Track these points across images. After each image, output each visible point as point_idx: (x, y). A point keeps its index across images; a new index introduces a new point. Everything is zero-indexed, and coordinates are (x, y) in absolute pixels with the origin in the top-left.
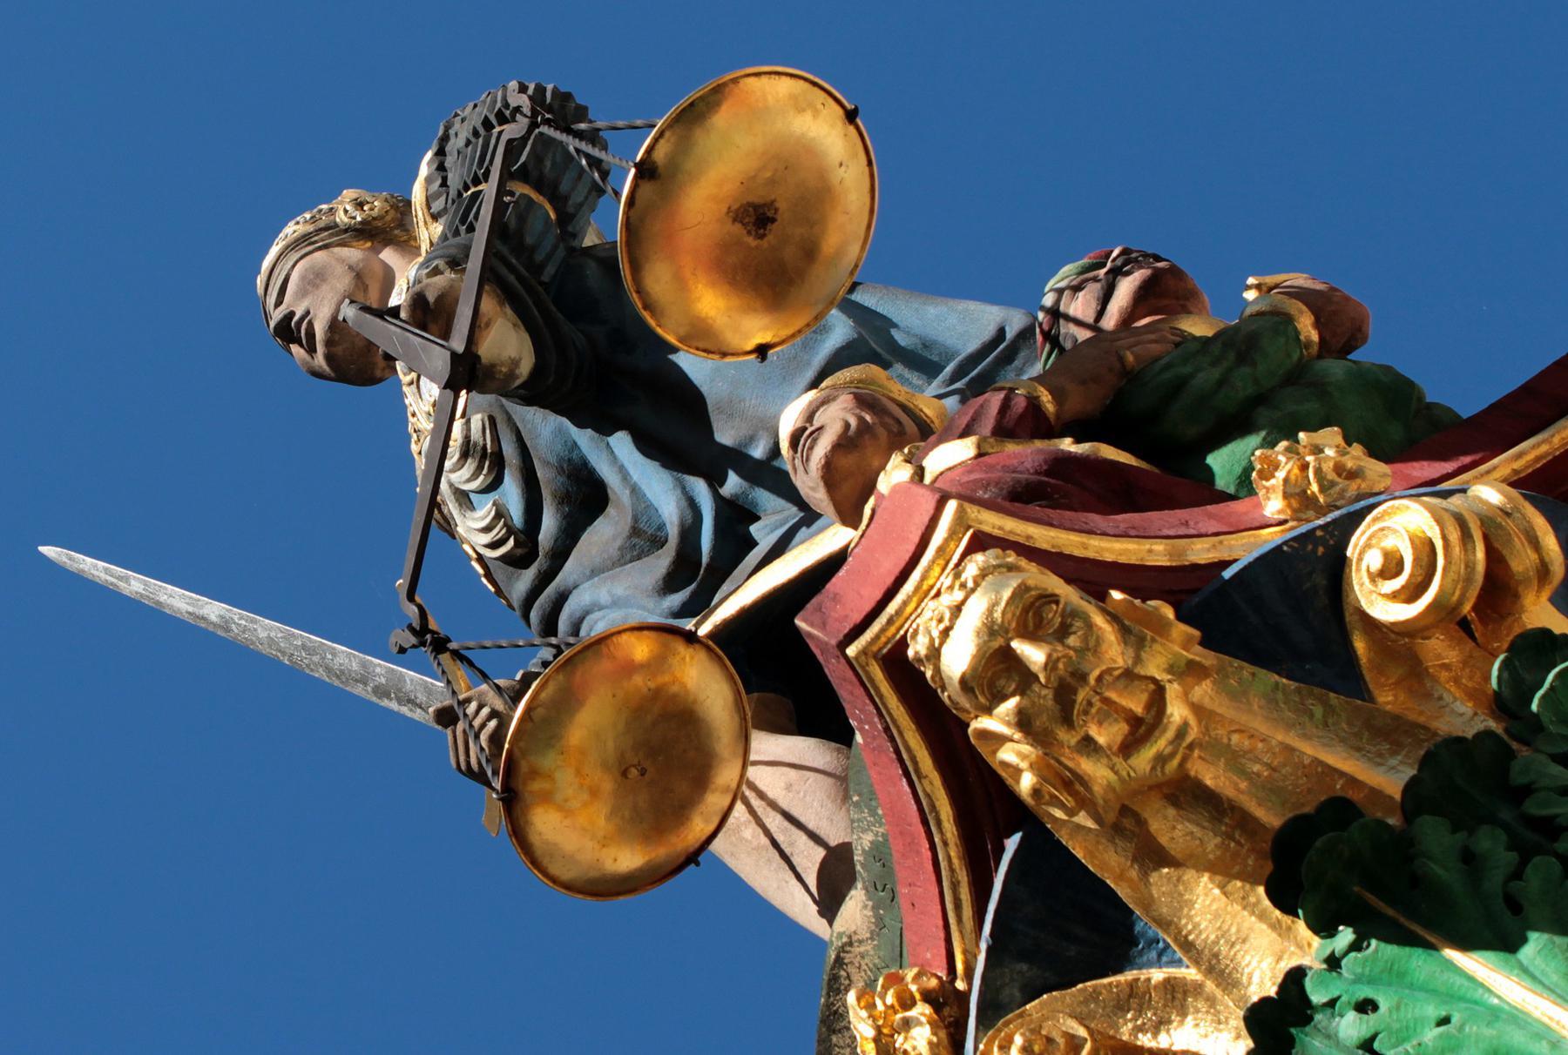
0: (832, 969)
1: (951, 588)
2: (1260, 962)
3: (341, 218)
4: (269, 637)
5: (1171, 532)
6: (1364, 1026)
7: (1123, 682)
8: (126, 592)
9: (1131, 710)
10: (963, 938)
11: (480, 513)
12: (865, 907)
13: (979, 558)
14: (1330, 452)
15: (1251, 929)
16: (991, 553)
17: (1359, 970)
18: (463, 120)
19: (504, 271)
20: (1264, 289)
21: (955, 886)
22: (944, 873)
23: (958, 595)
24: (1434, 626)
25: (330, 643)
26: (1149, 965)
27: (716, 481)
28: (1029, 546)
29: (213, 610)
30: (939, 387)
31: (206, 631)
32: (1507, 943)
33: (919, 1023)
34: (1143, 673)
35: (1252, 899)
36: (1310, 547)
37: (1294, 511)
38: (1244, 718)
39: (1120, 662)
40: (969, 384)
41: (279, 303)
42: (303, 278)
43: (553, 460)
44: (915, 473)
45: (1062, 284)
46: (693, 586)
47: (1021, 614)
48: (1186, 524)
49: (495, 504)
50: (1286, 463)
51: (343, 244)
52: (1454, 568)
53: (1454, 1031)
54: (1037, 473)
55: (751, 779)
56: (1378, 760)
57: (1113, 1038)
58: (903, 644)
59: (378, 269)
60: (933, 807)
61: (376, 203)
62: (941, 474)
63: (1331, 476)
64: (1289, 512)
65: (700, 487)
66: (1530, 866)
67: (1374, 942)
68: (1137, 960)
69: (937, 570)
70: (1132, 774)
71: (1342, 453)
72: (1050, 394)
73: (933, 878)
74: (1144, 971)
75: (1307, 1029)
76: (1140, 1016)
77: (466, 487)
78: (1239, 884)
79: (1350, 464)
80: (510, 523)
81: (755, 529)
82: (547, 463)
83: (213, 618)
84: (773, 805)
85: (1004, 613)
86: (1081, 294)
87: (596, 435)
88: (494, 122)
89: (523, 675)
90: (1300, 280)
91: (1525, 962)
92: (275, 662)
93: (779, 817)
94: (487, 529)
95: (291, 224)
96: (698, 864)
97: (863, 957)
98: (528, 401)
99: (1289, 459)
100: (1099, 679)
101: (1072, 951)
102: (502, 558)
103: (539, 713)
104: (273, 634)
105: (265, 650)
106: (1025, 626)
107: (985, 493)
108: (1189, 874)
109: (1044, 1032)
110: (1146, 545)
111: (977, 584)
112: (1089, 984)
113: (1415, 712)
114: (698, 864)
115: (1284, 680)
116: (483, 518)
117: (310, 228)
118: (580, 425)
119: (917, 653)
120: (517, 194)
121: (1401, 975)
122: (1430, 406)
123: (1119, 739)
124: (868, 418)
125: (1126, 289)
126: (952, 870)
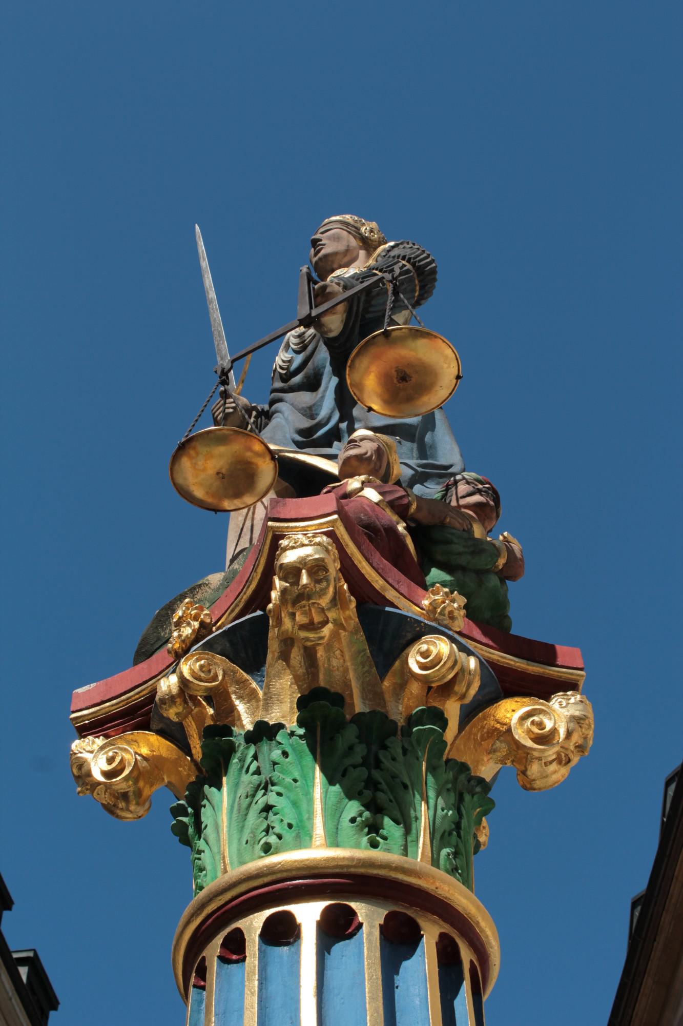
0: (196, 586)
1: (309, 538)
2: (278, 712)
3: (363, 229)
4: (215, 318)
5: (391, 581)
6: (279, 758)
7: (319, 610)
8: (201, 263)
9: (313, 619)
10: (226, 619)
11: (287, 355)
12: (220, 581)
13: (325, 538)
14: (456, 605)
15: (285, 702)
16: (329, 540)
17: (294, 743)
18: (404, 248)
19: (355, 303)
20: (506, 539)
21: (237, 606)
22: (238, 599)
23: (306, 542)
24: (420, 681)
25: (225, 339)
26: (256, 680)
27: (341, 420)
28: (344, 548)
29: (212, 295)
30: (415, 463)
31: (206, 297)
32: (331, 781)
33: (191, 627)
34: (327, 614)
35: (295, 695)
36: (416, 625)
37: (429, 610)
38: (346, 650)
39: (324, 605)
40: (422, 472)
41: (322, 233)
42: (334, 234)
43: (316, 364)
44: (360, 488)
45: (467, 477)
46: (305, 440)
47: (314, 565)
48: (398, 582)
49: (292, 357)
50: (441, 596)
51: (355, 237)
52: (438, 673)
53: (294, 787)
54: (382, 526)
55: (257, 506)
56: (364, 698)
57: (228, 687)
58: (282, 537)
59: (355, 254)
60: (251, 582)
61: (376, 236)
62: (364, 497)
63: (446, 612)
64: (427, 608)
65: (336, 416)
66: (360, 768)
67: (305, 742)
68: (254, 676)
69: (314, 528)
70: (297, 634)
71: (459, 608)
72: (417, 507)
73: (235, 597)
74: (253, 681)
75: (268, 742)
76: (240, 689)
77: (291, 344)
78: (296, 688)
79: (456, 613)
80: (290, 367)
81: (336, 443)
82: (313, 364)
83: (210, 296)
84: (253, 519)
85: (310, 560)
86: (467, 486)
87: (331, 371)
88: (406, 259)
89: (255, 406)
90: (516, 547)
91: (329, 789)
92: (210, 326)
93: (250, 524)
94: (284, 361)
95: (350, 216)
96: (216, 513)
97: (206, 592)
98: (326, 344)
99: (442, 596)
100: (314, 603)
101: (243, 655)
102: (280, 373)
103: (212, 435)
104: (217, 319)
105: (212, 320)
106: (312, 570)
107: (363, 516)
108: (288, 671)
109: (211, 667)
110: (378, 578)
111: (314, 545)
112: (237, 667)
113: (388, 697)
114: (216, 513)
115: (368, 651)
116: (286, 357)
117: (352, 223)
118: (331, 364)
119: (282, 544)
120: (385, 287)
121: (301, 757)
122: (507, 617)
123: (302, 623)
124: (374, 457)
125: (477, 498)
126: (240, 601)
